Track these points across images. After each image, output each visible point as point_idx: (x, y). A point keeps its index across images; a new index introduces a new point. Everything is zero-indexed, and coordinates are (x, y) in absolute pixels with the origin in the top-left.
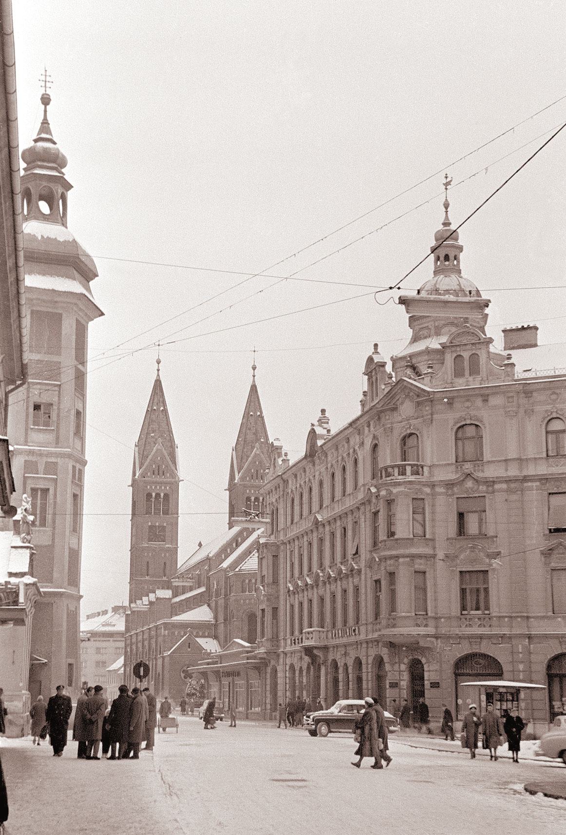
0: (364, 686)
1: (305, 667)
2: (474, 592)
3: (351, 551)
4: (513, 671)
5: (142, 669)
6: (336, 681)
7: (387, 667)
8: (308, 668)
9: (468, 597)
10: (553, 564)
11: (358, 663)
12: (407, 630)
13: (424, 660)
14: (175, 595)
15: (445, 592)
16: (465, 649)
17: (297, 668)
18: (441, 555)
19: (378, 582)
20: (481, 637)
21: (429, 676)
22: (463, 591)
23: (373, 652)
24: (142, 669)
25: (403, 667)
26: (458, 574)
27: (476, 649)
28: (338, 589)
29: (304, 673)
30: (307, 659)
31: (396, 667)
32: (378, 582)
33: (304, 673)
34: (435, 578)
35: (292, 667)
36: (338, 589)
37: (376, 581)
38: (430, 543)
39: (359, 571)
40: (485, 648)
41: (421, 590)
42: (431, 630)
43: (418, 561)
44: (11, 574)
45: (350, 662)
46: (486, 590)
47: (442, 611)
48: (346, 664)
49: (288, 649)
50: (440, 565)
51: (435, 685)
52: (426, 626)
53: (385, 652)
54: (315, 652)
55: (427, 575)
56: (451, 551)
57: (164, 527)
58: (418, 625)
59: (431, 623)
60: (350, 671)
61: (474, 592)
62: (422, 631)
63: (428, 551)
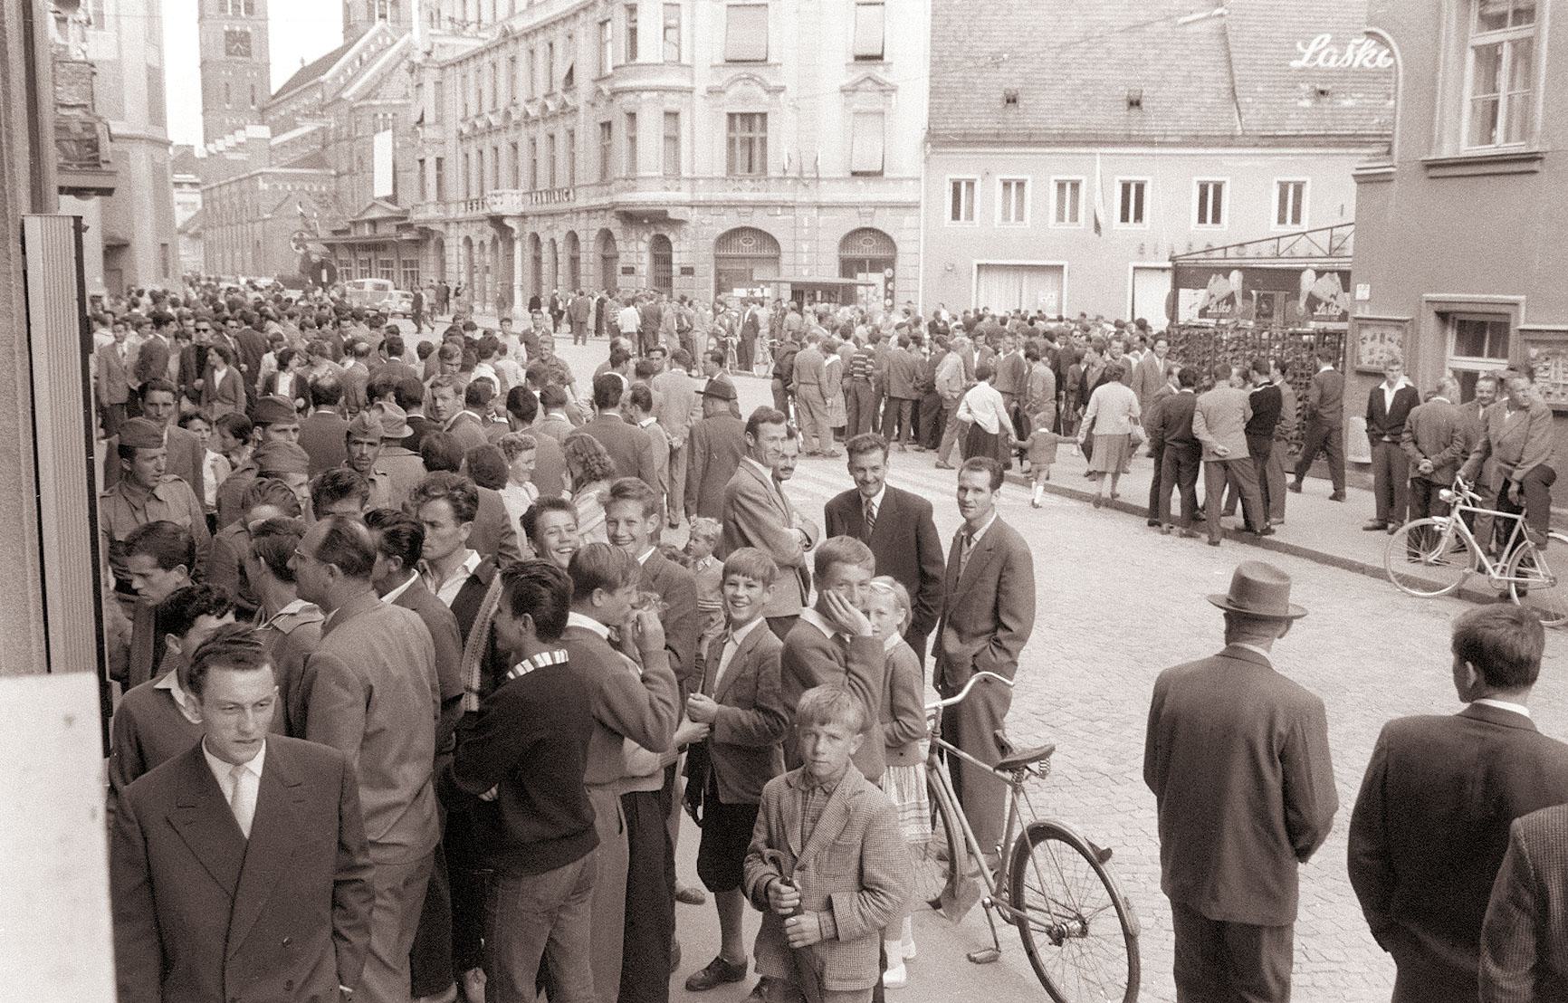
0: (583, 268)
1: (488, 242)
2: (747, 132)
3: (560, 73)
4: (818, 178)
5: (324, 272)
6: (537, 260)
7: (620, 246)
8: (495, 242)
9: (738, 152)
10: (856, 106)
11: (573, 238)
12: (647, 196)
13: (672, 237)
14: (274, 135)
15: (706, 143)
16: (731, 221)
17: (476, 242)
18: (701, 89)
19: (607, 126)
20: (755, 206)
21: (678, 260)
22: (731, 142)
23: (597, 224)
24: (324, 272)
25: (643, 246)
26: (725, 118)
27: (745, 222)
28: (541, 133)
29: (488, 249)
30: (491, 231)
31: (632, 246)
32: (607, 126)
33: (488, 249)
34: (692, 119)
35: (468, 241)
36: (541, 133)
37: (603, 125)
38: (687, 70)
39: (576, 110)
40: (759, 220)
41: (672, 139)
42: (685, 196)
43: (670, 96)
44: (335, 232)
45: (560, 238)
46: (764, 141)
47: (702, 168)
48: (553, 240)
49: (460, 215)
50: (699, 102)
51: (688, 271)
52: (678, 189)
53: (615, 226)
54: (507, 222)
55: (681, 116)
56: (717, 83)
57: (247, 34)
58: (667, 189)
59: (686, 186)
60: (560, 247)
61: (747, 132)
62: (672, 196)
63: (686, 83)
